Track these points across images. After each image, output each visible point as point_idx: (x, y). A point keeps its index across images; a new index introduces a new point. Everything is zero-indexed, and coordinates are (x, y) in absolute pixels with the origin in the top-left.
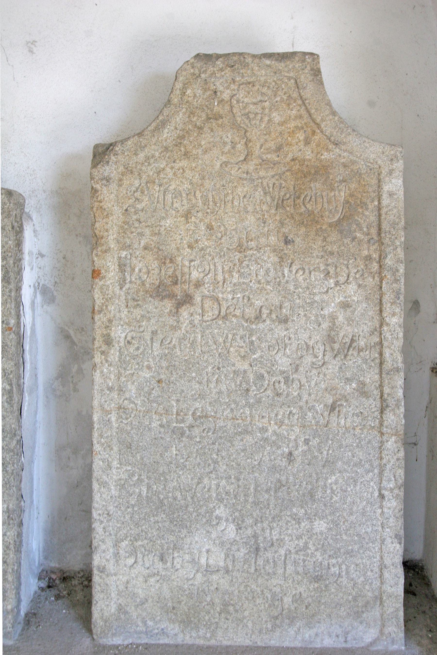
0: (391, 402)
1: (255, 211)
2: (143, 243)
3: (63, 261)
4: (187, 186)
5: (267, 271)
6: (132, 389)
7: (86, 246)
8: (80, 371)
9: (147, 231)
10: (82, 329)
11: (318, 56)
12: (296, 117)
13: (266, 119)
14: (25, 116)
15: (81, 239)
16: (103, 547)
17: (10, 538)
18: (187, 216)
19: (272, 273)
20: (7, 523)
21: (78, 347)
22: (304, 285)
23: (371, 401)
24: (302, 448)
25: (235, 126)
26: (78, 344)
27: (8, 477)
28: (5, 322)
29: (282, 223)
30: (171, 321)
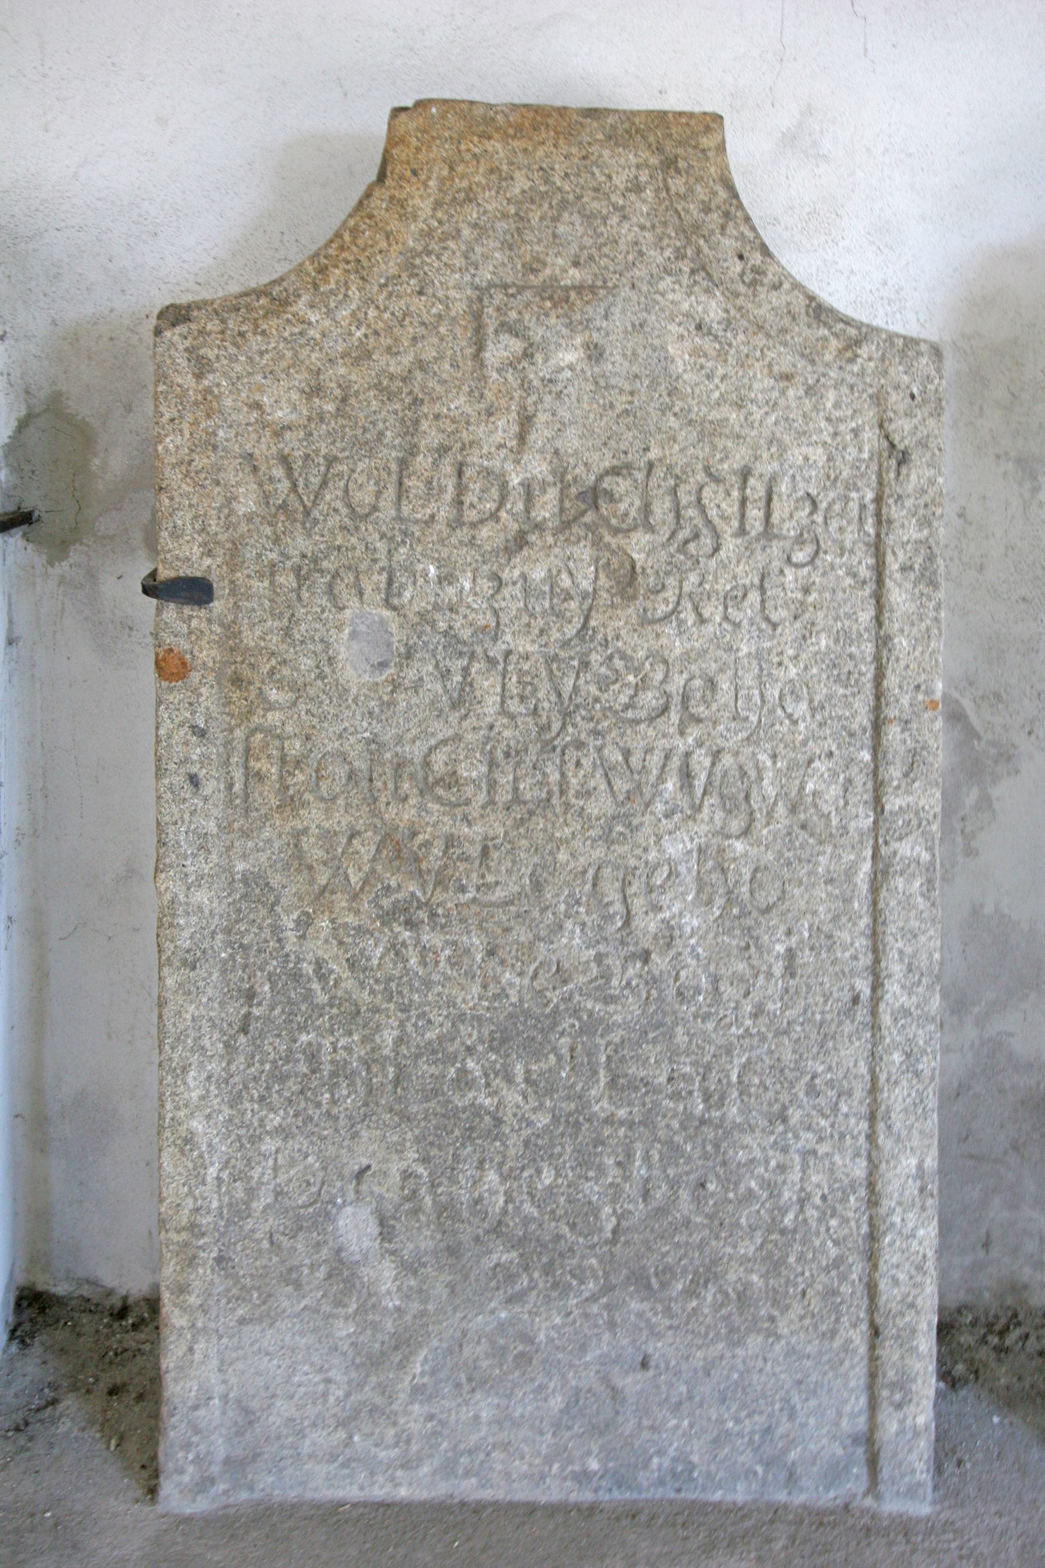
3: (958, 523)
7: (1020, 484)
8: (985, 803)
10: (997, 696)
14: (886, 150)
15: (1010, 466)
17: (926, 1243)
20: (918, 1205)
21: (983, 743)
26: (982, 734)
27: (920, 1087)
28: (923, 687)
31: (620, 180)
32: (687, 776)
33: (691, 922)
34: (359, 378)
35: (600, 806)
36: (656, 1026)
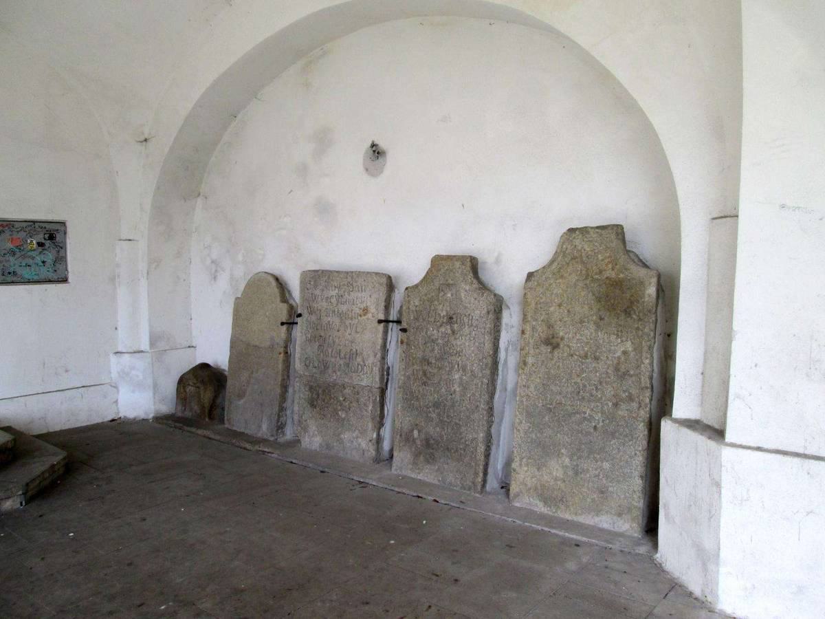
0: (643, 404)
1: (588, 304)
2: (542, 318)
4: (561, 291)
5: (591, 333)
6: (532, 386)
9: (544, 313)
11: (621, 226)
12: (608, 257)
13: (596, 258)
16: (516, 460)
18: (560, 305)
19: (594, 335)
22: (607, 341)
23: (634, 404)
24: (601, 424)
25: (583, 262)
29: (599, 310)
30: (550, 356)
31: (458, 267)
32: (458, 365)
33: (458, 390)
34: (425, 298)
35: (447, 369)
36: (453, 406)
